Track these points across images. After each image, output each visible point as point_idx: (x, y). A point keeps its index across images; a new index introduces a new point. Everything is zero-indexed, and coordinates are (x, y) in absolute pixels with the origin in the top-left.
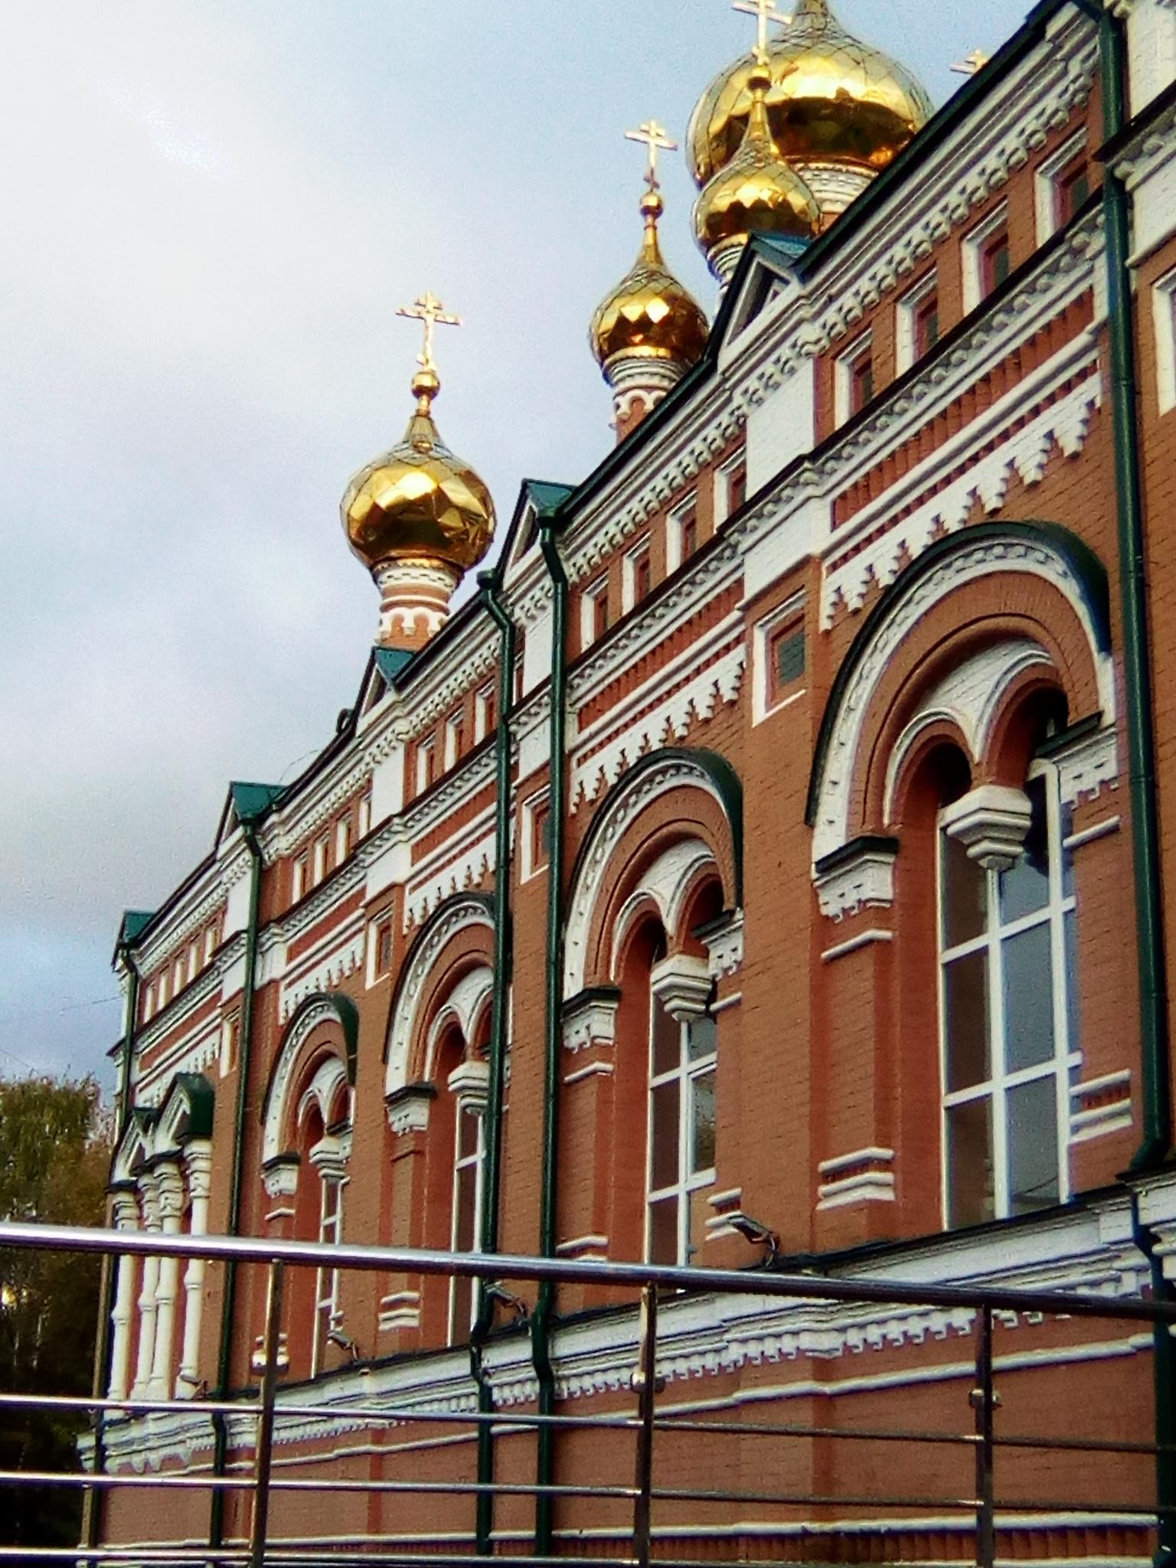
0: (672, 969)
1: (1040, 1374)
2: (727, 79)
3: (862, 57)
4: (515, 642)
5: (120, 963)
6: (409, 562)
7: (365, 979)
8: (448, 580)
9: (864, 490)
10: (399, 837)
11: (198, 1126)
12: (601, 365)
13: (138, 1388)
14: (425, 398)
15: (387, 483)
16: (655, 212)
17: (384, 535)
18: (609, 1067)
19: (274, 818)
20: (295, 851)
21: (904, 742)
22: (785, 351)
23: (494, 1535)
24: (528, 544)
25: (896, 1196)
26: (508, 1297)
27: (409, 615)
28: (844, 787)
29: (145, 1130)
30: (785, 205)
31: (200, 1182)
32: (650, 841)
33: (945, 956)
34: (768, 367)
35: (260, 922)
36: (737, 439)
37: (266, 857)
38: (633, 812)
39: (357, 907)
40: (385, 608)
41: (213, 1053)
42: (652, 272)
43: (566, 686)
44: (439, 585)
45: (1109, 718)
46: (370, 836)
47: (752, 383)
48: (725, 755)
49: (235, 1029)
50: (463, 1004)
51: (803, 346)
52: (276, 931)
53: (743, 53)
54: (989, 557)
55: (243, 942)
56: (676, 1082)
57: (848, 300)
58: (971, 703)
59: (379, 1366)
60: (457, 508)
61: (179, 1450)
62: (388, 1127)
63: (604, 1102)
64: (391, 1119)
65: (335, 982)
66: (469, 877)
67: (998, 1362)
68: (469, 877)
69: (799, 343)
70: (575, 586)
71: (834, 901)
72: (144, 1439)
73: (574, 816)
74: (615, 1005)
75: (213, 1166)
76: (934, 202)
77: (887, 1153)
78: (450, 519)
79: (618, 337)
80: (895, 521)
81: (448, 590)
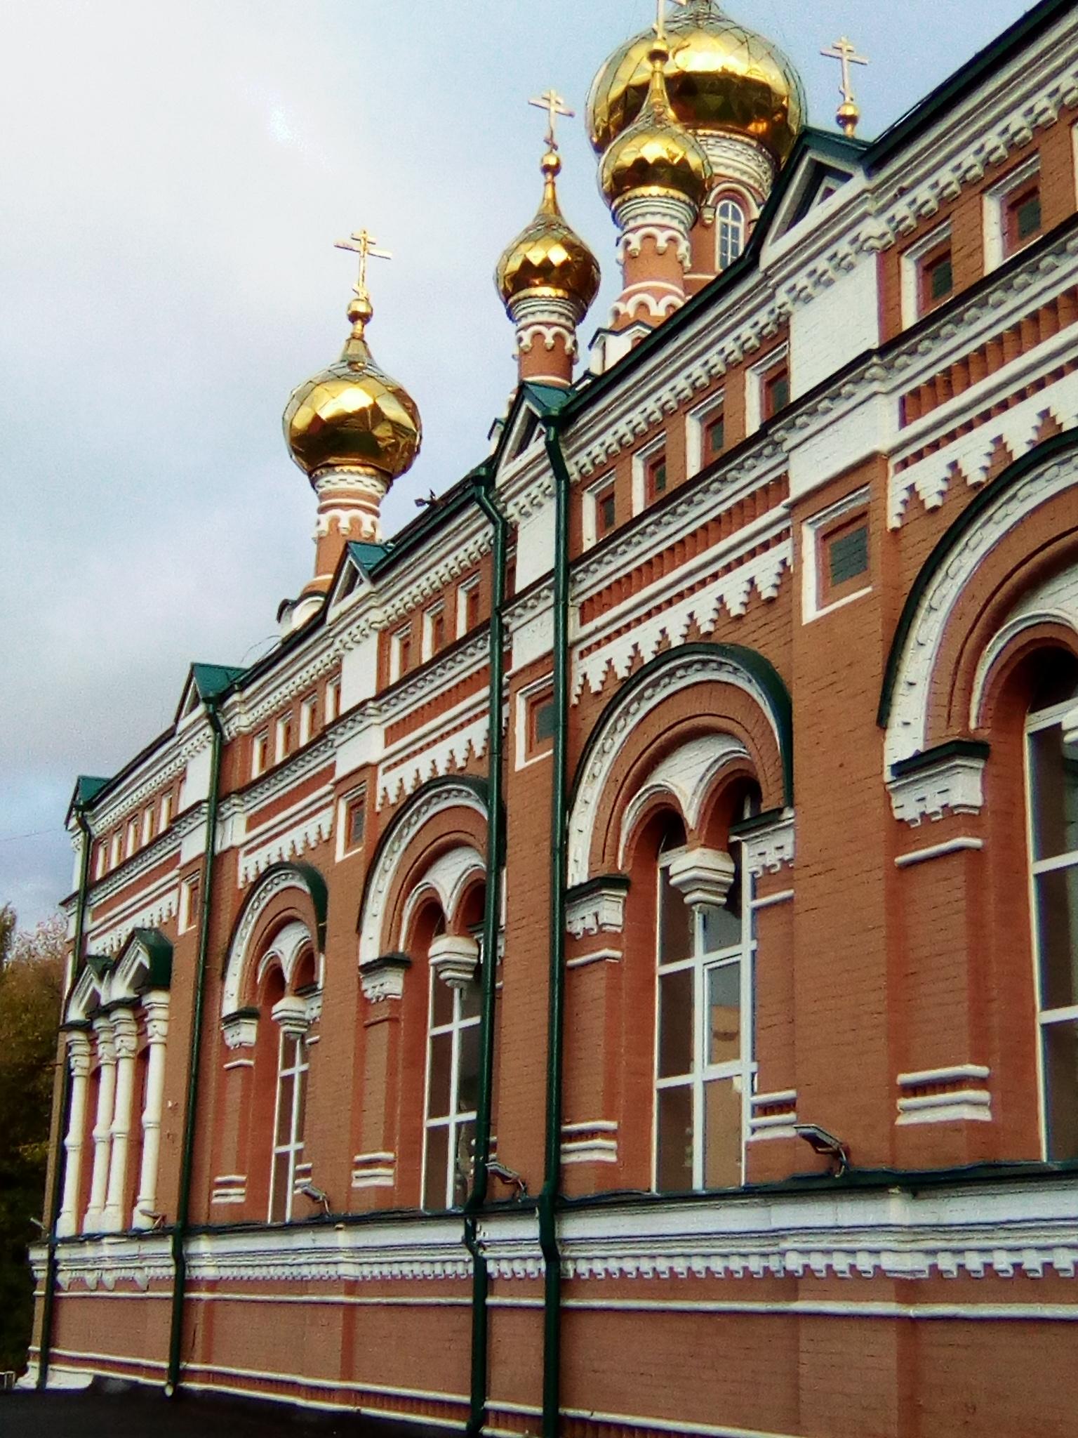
0: (689, 863)
2: (624, 54)
3: (747, 40)
4: (508, 535)
5: (73, 822)
6: (346, 468)
7: (335, 852)
8: (380, 487)
9: (945, 385)
10: (373, 720)
11: (157, 976)
12: (506, 303)
13: (92, 1212)
14: (359, 323)
15: (327, 396)
16: (552, 170)
17: (320, 445)
18: (618, 954)
19: (235, 697)
20: (254, 729)
21: (996, 644)
22: (843, 247)
23: (489, 1404)
24: (522, 446)
25: (993, 1115)
26: (510, 1175)
27: (345, 517)
28: (922, 689)
29: (101, 978)
30: (684, 162)
31: (157, 1029)
32: (670, 733)
33: (1037, 867)
34: (821, 264)
35: (221, 793)
37: (226, 733)
39: (325, 783)
40: (322, 510)
41: (170, 911)
42: (549, 223)
43: (569, 580)
44: (372, 490)
46: (339, 720)
47: (801, 280)
48: (761, 651)
49: (193, 890)
50: (442, 882)
51: (866, 240)
52: (236, 801)
53: (644, 28)
55: (205, 810)
56: (689, 973)
57: (923, 193)
59: (355, 1222)
60: (391, 422)
61: (138, 1275)
62: (362, 992)
64: (364, 986)
65: (299, 852)
66: (452, 761)
68: (452, 761)
69: (862, 238)
70: (577, 484)
71: (909, 805)
72: (100, 1259)
73: (575, 706)
74: (624, 894)
75: (171, 1015)
77: (982, 1071)
78: (381, 431)
79: (518, 282)
80: (659, 609)
81: (379, 495)
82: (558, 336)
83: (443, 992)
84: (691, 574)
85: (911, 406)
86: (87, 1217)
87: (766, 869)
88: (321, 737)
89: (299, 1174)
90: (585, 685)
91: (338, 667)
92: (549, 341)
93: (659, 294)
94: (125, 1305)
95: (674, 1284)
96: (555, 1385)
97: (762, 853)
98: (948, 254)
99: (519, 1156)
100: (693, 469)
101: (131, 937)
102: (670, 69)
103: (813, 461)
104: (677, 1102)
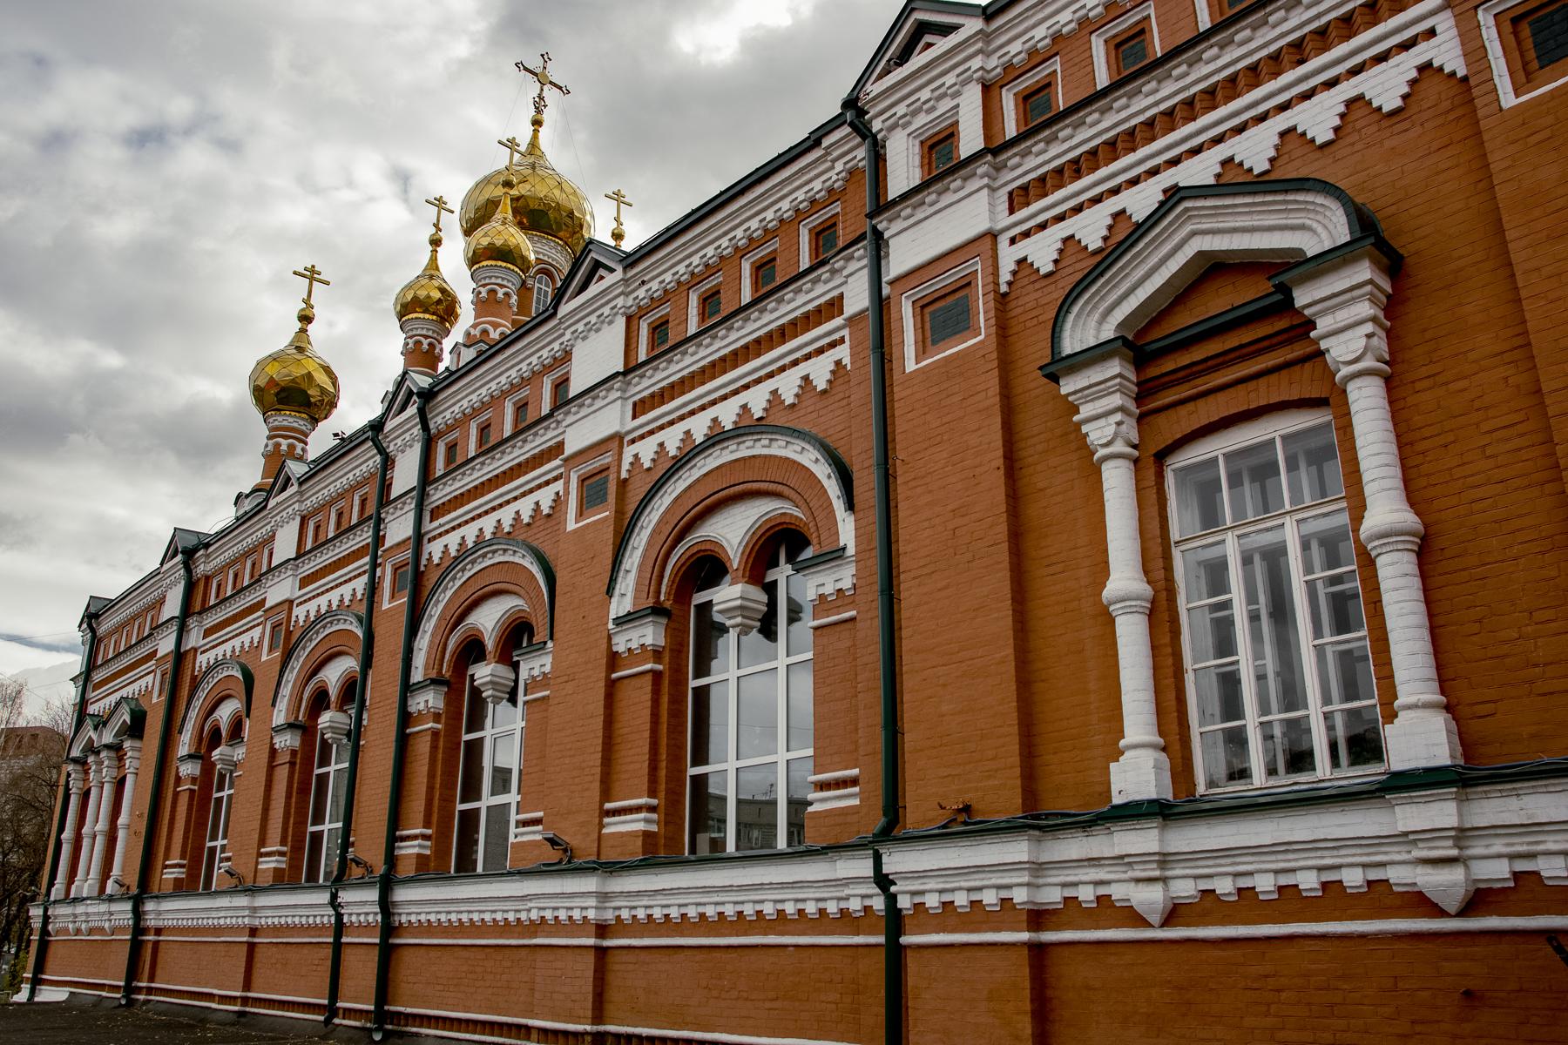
0: (483, 673)
1: (747, 951)
4: (388, 462)
24: (403, 409)
34: (593, 319)
36: (567, 356)
38: (468, 574)
45: (851, 551)
54: (758, 444)
57: (654, 285)
58: (732, 531)
62: (272, 745)
63: (434, 748)
67: (344, 940)
76: (726, 233)
80: (480, 516)
82: (430, 344)
83: (326, 746)
84: (501, 495)
85: (639, 408)
86: (73, 887)
87: (821, 596)
88: (257, 581)
89: (221, 860)
90: (430, 559)
91: (273, 538)
92: (425, 346)
93: (496, 326)
94: (92, 945)
95: (460, 929)
96: (383, 991)
97: (534, 666)
98: (667, 322)
99: (369, 848)
100: (507, 432)
101: (118, 704)
102: (514, 192)
103: (580, 433)
104: (469, 819)
